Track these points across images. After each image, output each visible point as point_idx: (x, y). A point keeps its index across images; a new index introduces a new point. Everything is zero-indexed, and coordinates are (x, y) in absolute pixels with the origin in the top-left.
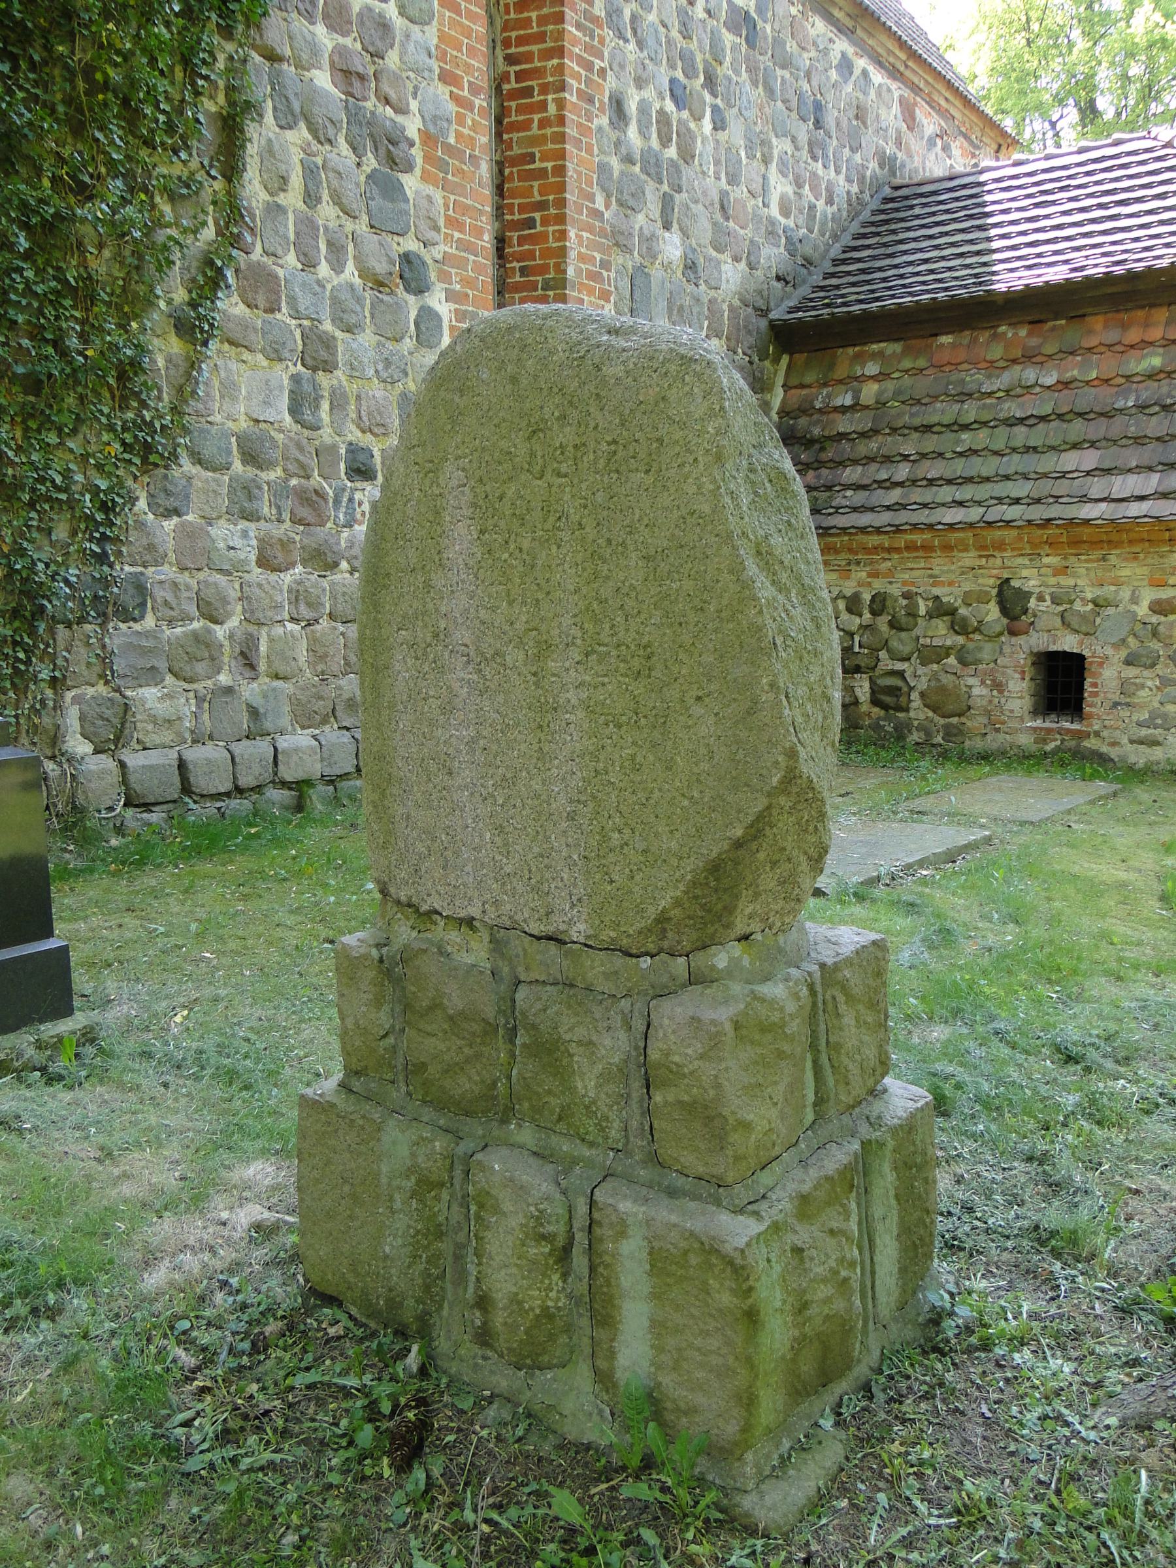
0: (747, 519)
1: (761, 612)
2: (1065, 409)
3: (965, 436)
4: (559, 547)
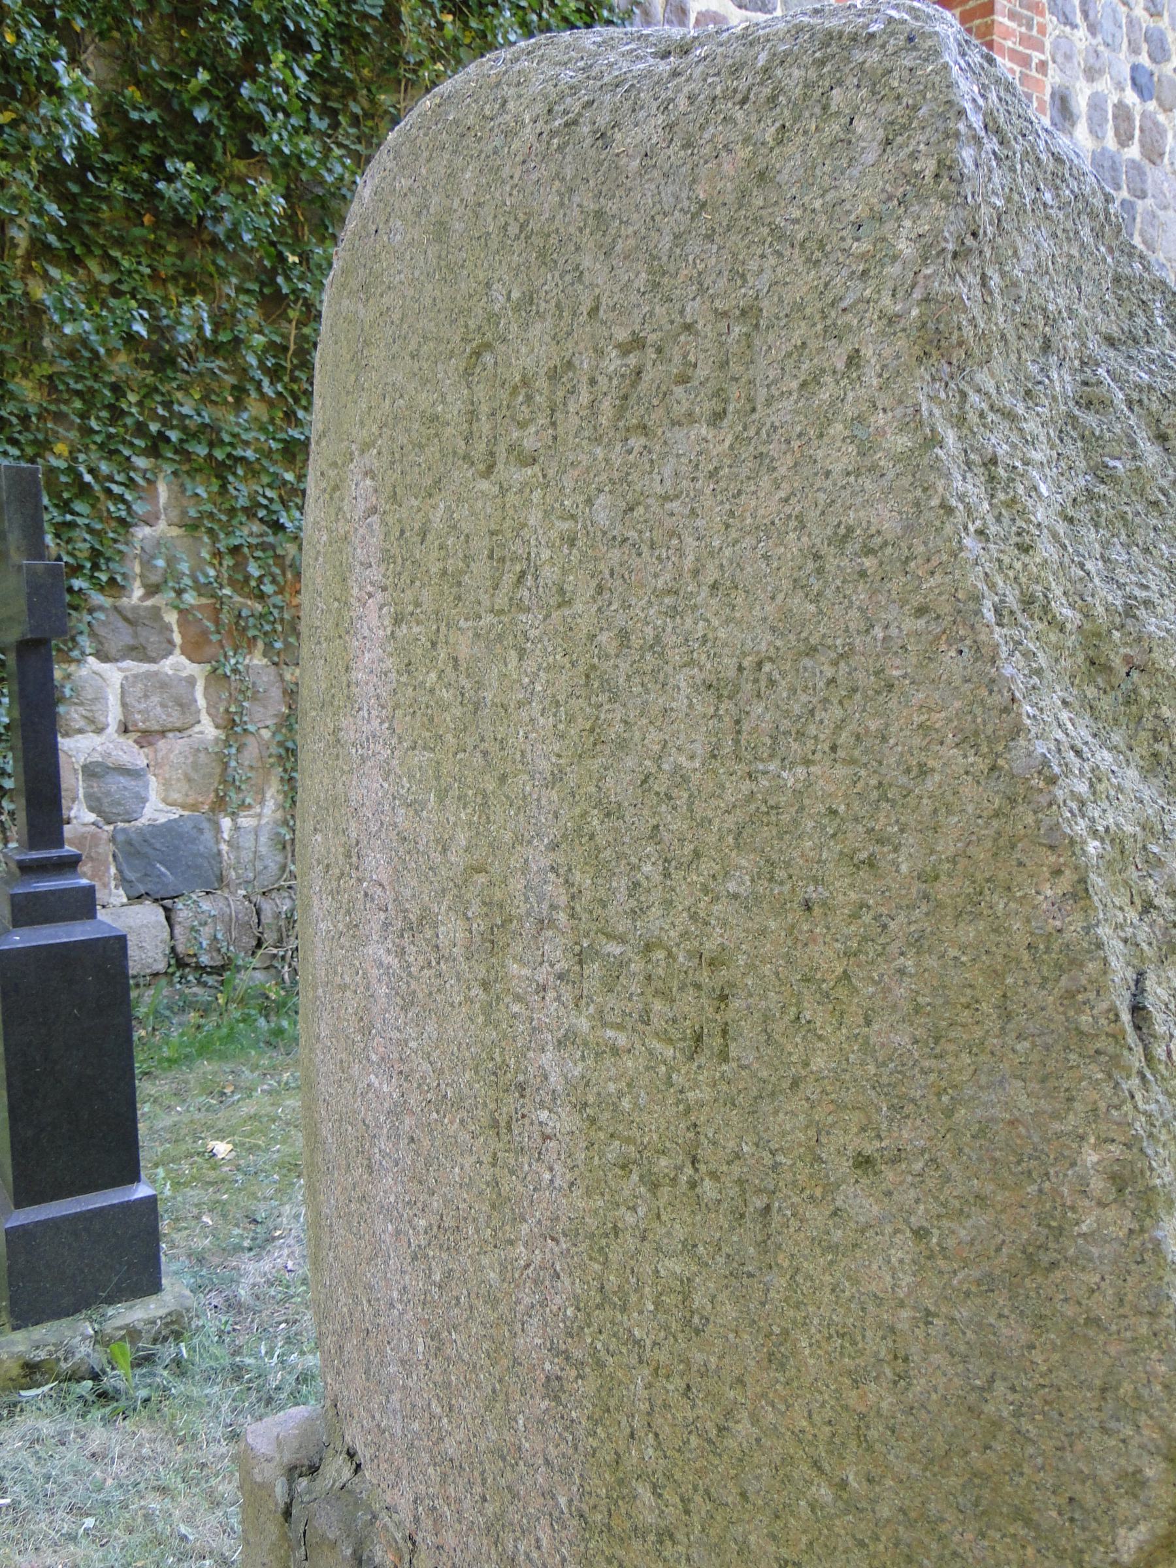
0: (1046, 550)
1: (1080, 893)
4: (522, 654)
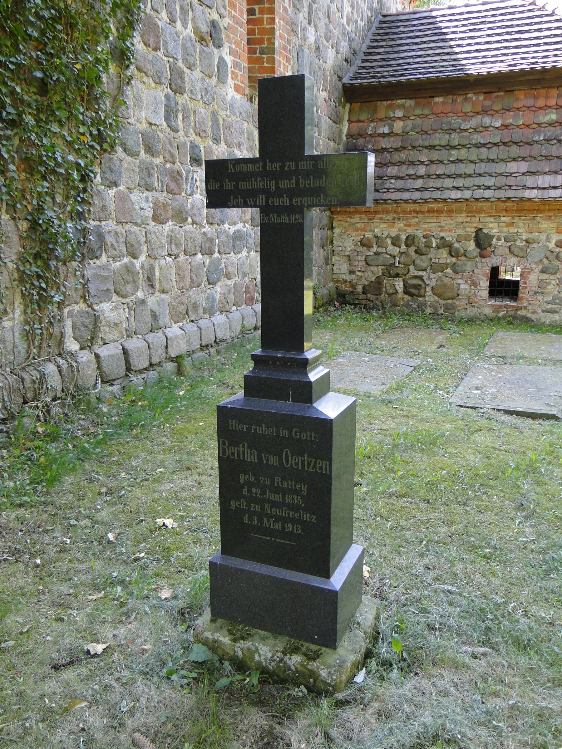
2: (507, 140)
3: (454, 152)
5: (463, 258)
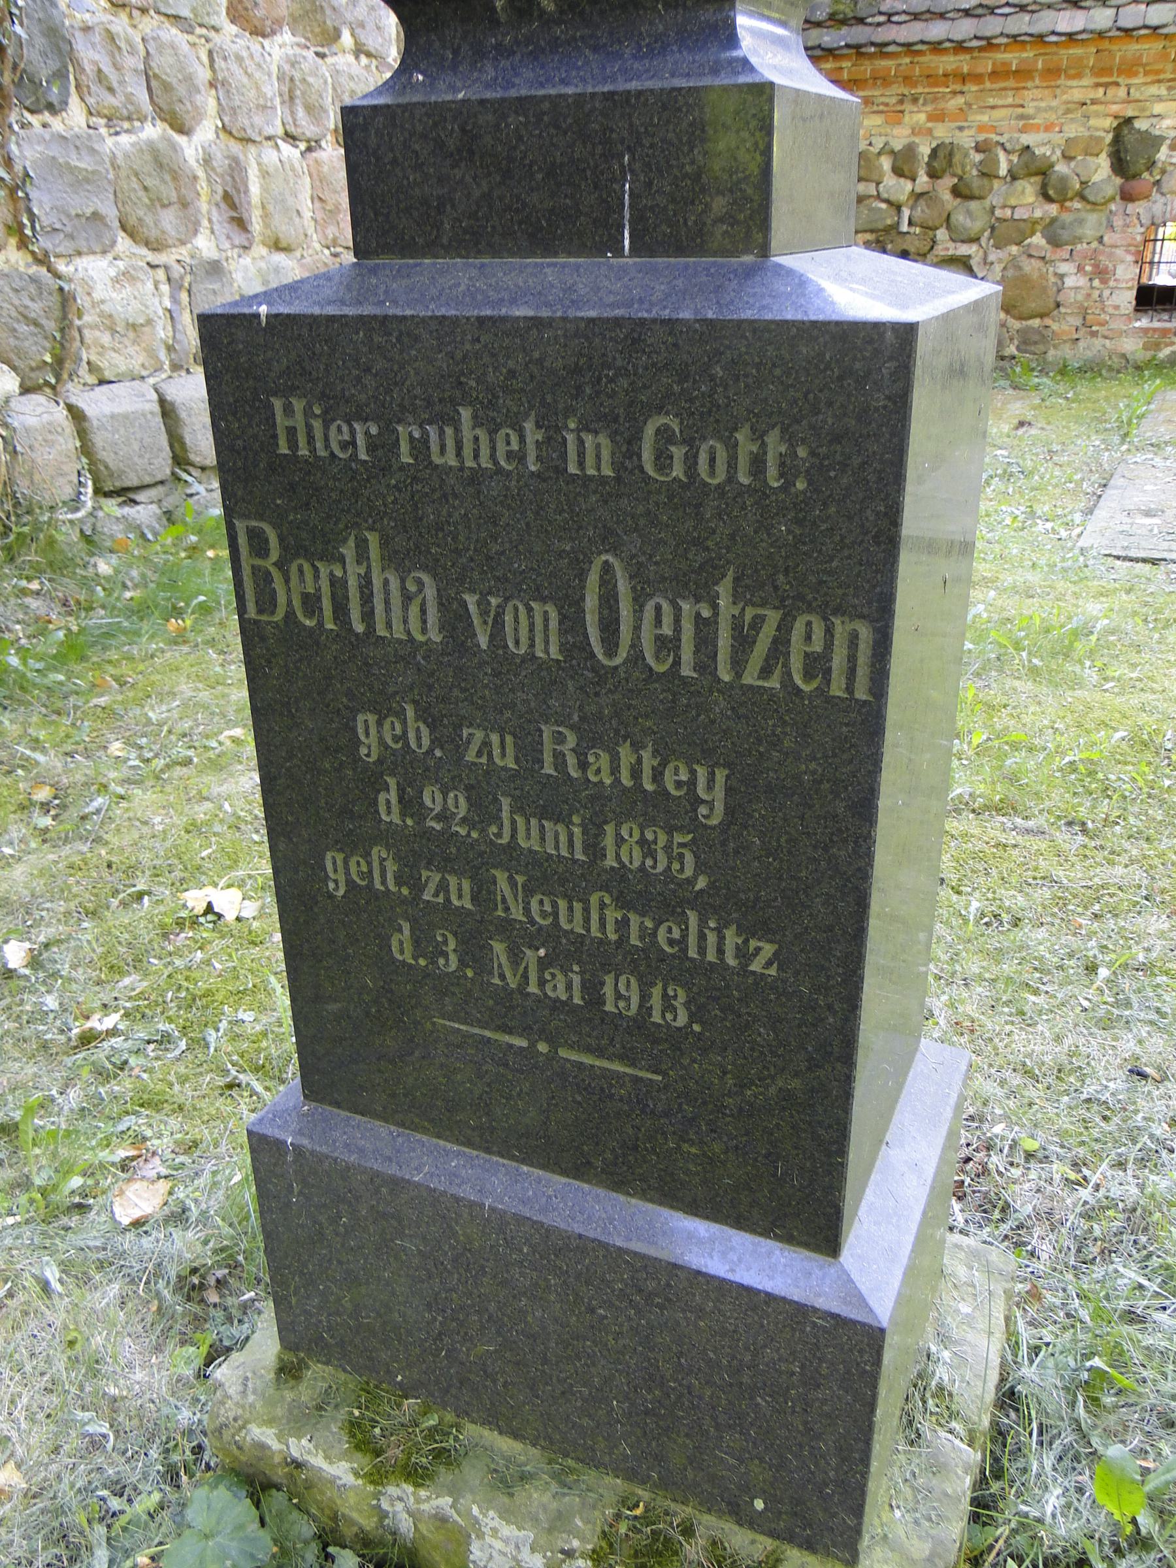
5: (1077, 205)
